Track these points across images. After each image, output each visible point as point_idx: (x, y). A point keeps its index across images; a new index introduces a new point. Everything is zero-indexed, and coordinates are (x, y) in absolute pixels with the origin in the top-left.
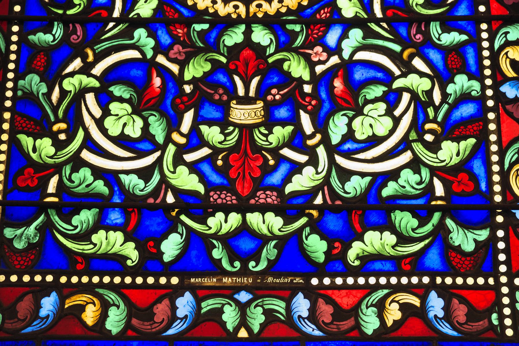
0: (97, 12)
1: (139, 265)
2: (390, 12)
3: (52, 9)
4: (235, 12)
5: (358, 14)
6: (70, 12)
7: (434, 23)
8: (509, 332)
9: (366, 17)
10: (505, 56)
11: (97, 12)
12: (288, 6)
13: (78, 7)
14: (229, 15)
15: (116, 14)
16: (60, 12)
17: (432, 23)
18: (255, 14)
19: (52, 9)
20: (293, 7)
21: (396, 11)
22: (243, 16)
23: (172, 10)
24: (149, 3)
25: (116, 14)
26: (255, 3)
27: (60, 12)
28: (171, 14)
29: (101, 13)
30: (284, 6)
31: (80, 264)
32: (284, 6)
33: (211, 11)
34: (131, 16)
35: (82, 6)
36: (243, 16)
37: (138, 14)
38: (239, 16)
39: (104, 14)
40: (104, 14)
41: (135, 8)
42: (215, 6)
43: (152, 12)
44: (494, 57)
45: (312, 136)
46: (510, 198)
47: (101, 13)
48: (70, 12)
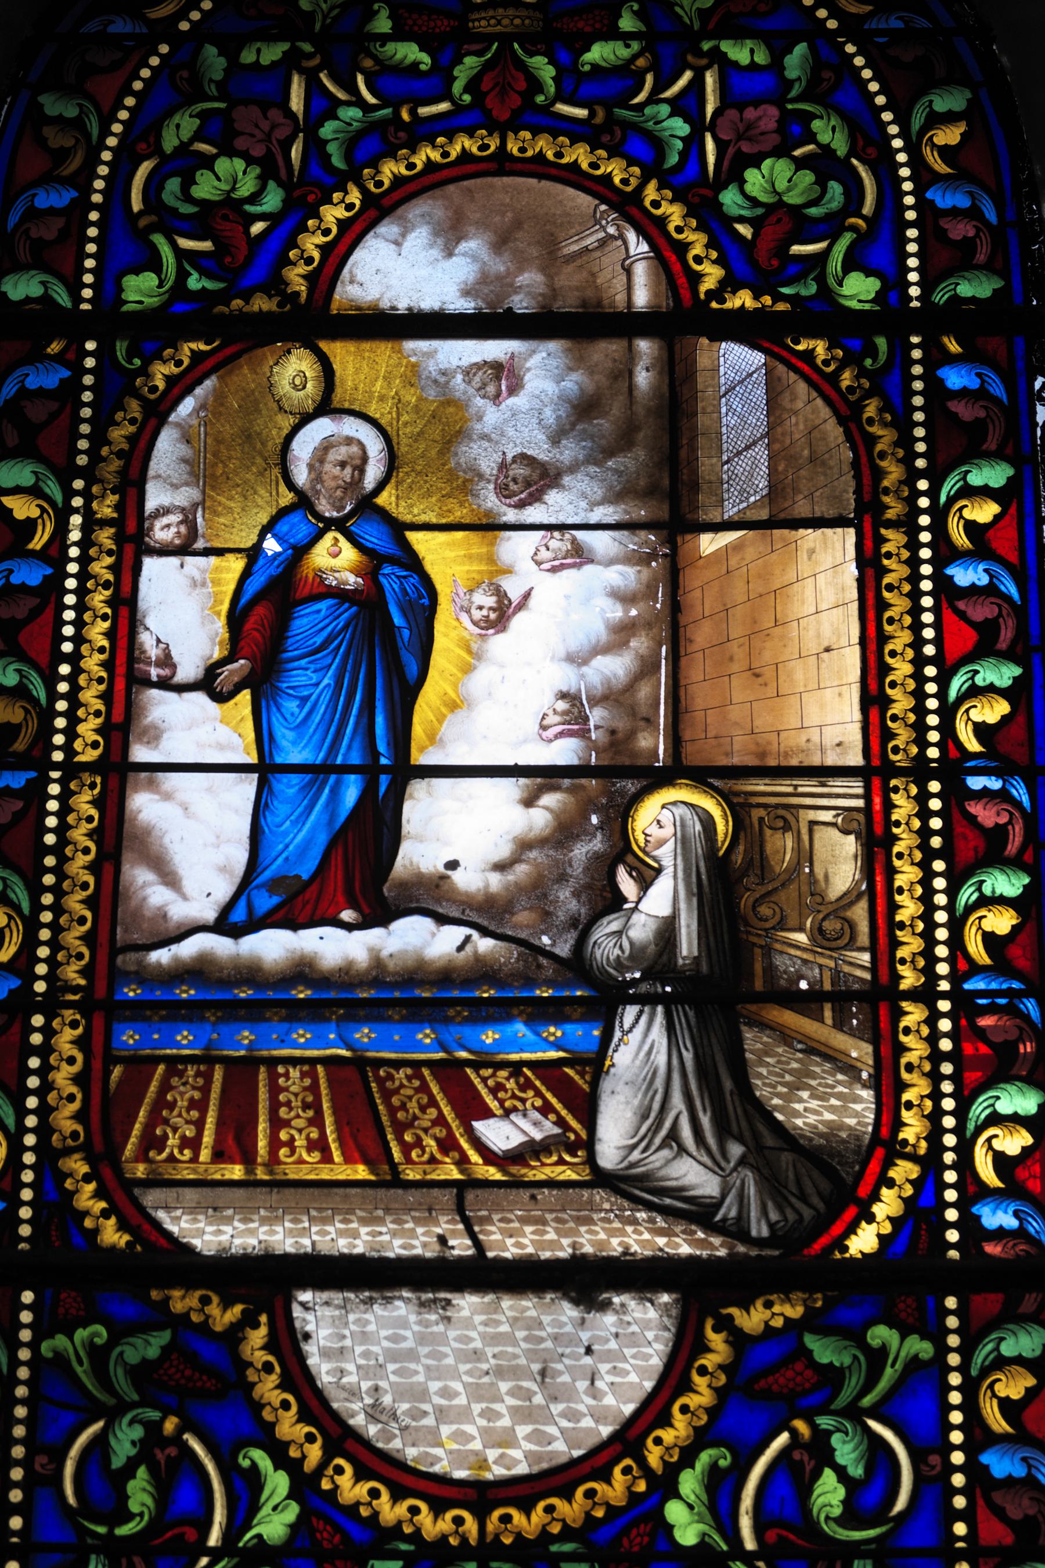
0: (176, 1531)
1: (766, 345)
2: (771, 1536)
3: (86, 1523)
4: (457, 1532)
5: (707, 1539)
6: (123, 1531)
7: (862, 1562)
8: (951, 1302)
9: (725, 1548)
10: (989, 1393)
11: (176, 1531)
12: (564, 1521)
13: (138, 1519)
14: (444, 1538)
15: (214, 1539)
16: (101, 1530)
17: (856, 1562)
18: (497, 1536)
19: (86, 1523)
20: (574, 1521)
21: (784, 1533)
22: (473, 1537)
23: (329, 1528)
24: (282, 1511)
25: (214, 1539)
26: (496, 1514)
27: (101, 1530)
28: (325, 1534)
29: (184, 1534)
30: (557, 1520)
31: (789, 174)
32: (557, 1520)
33: (408, 1530)
34: (241, 1544)
35: (146, 1518)
36: (473, 1537)
37: (259, 1536)
38: (464, 1539)
39: (191, 1534)
40: (191, 1534)
41: (255, 1522)
42: (415, 1519)
43: (288, 1530)
44: (956, 926)
45: (854, 228)
46: (953, 753)
47: (184, 1534)
48: (123, 1531)
